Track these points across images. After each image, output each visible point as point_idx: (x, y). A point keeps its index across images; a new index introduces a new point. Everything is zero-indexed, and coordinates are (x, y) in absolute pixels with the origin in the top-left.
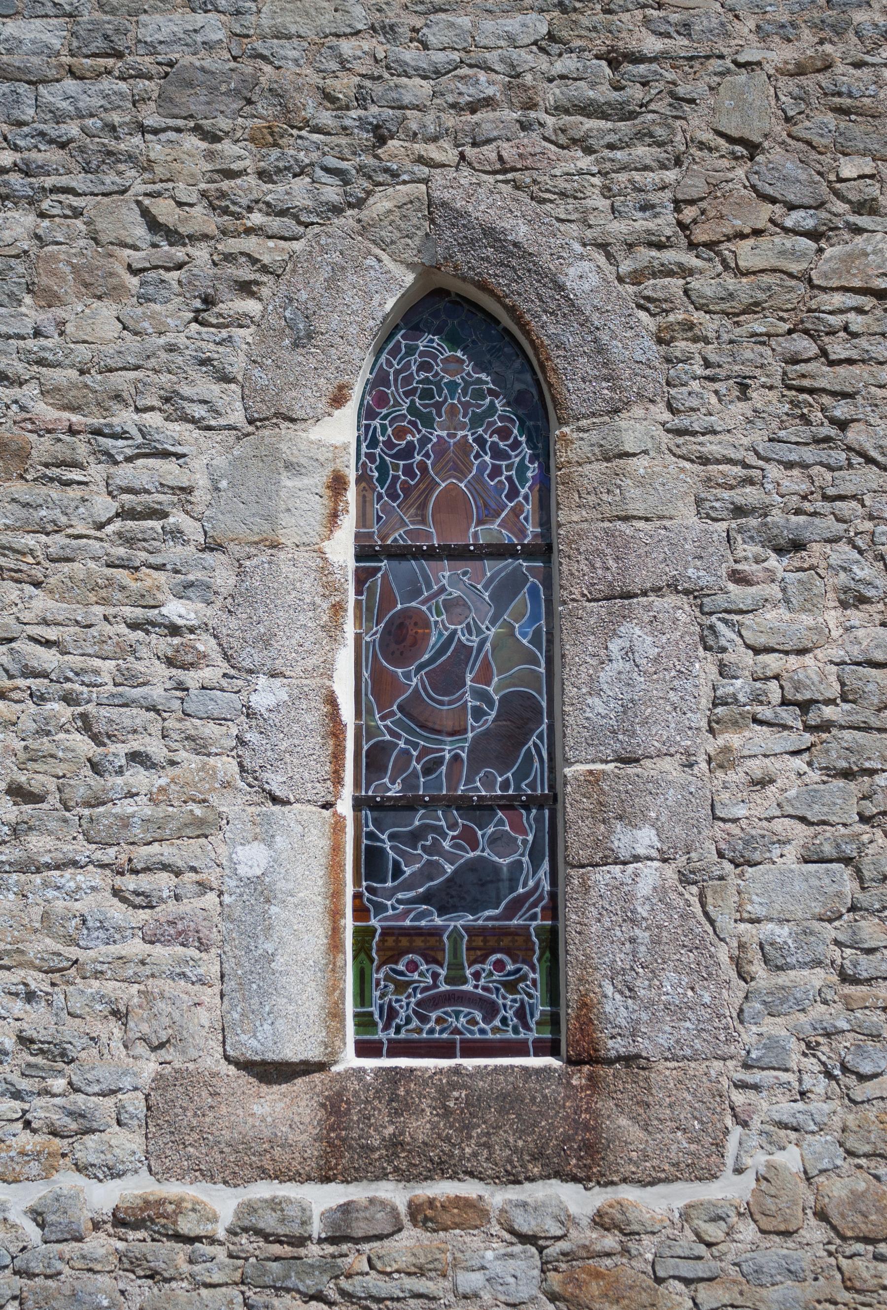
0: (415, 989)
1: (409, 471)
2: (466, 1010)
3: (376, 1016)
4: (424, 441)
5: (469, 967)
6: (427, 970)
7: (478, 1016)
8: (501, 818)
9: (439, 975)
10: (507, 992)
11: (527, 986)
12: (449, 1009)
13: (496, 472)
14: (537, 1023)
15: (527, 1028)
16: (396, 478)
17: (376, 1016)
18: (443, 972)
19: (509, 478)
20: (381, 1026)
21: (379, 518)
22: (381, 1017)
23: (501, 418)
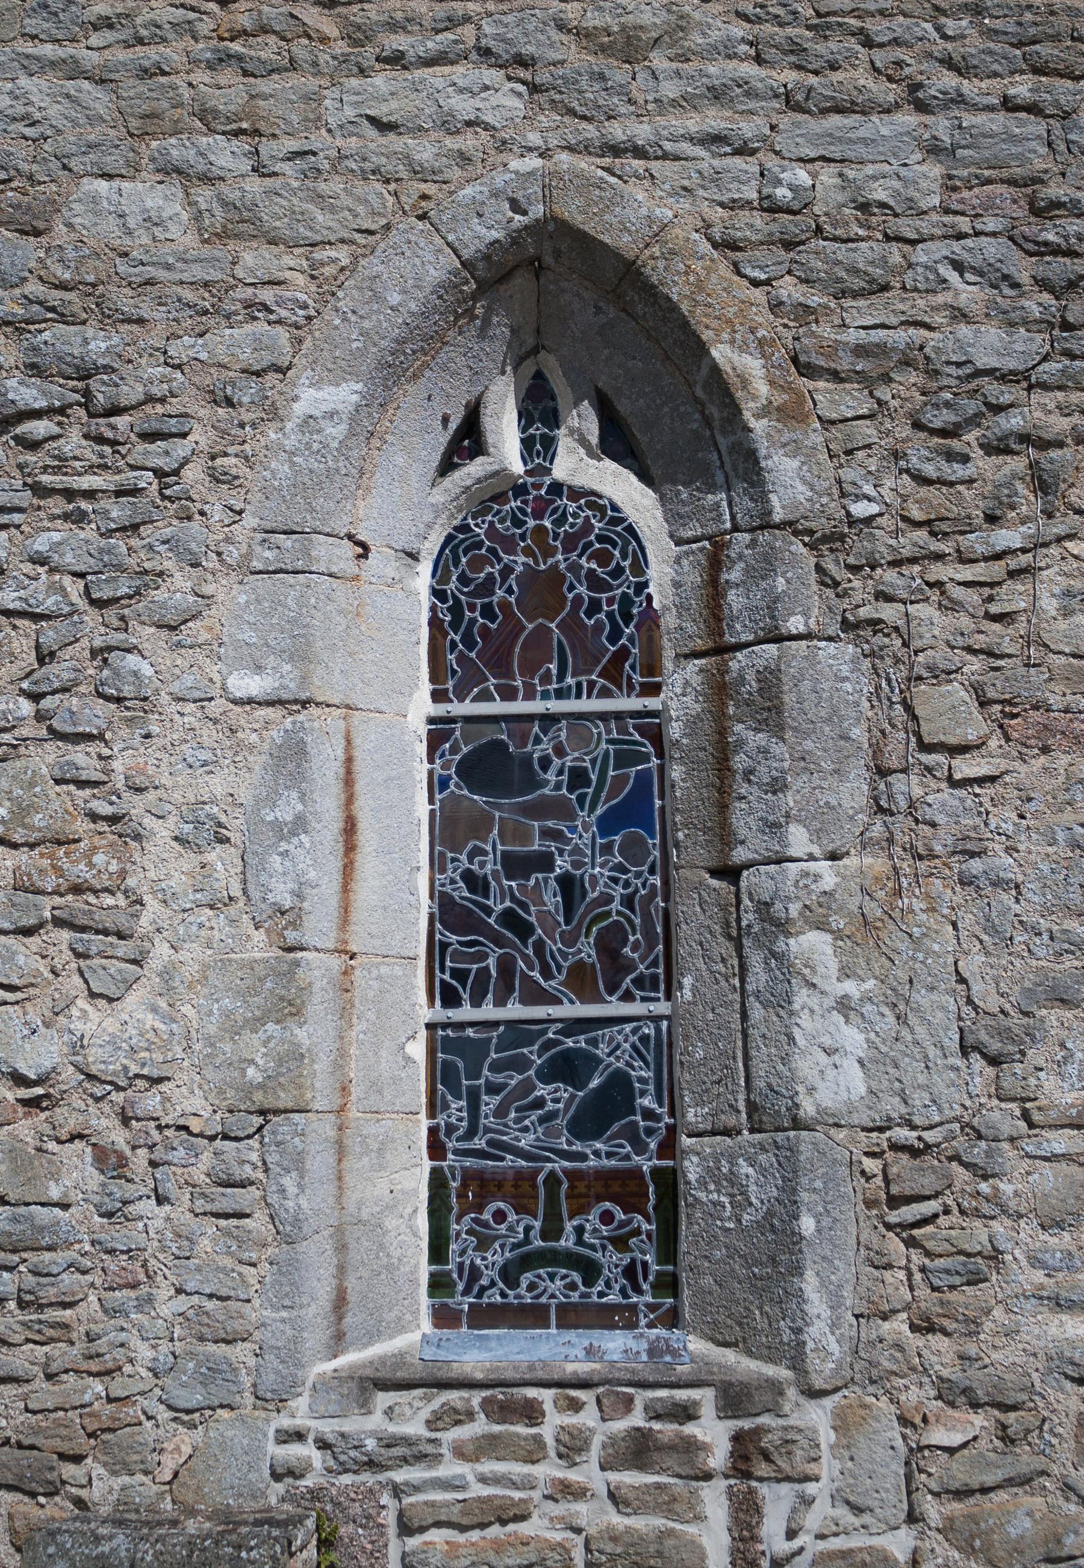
0: (502, 1246)
1: (488, 612)
2: (564, 1271)
3: (455, 1276)
4: (506, 571)
5: (571, 1218)
6: (518, 1222)
7: (576, 1277)
8: (604, 686)
9: (533, 1227)
10: (465, 757)
11: (642, 1241)
12: (541, 1271)
13: (594, 607)
14: (653, 1287)
15: (639, 1291)
16: (473, 621)
17: (455, 1276)
18: (537, 1224)
19: (610, 615)
20: (460, 1287)
21: (454, 672)
22: (460, 1277)
23: (601, 539)
